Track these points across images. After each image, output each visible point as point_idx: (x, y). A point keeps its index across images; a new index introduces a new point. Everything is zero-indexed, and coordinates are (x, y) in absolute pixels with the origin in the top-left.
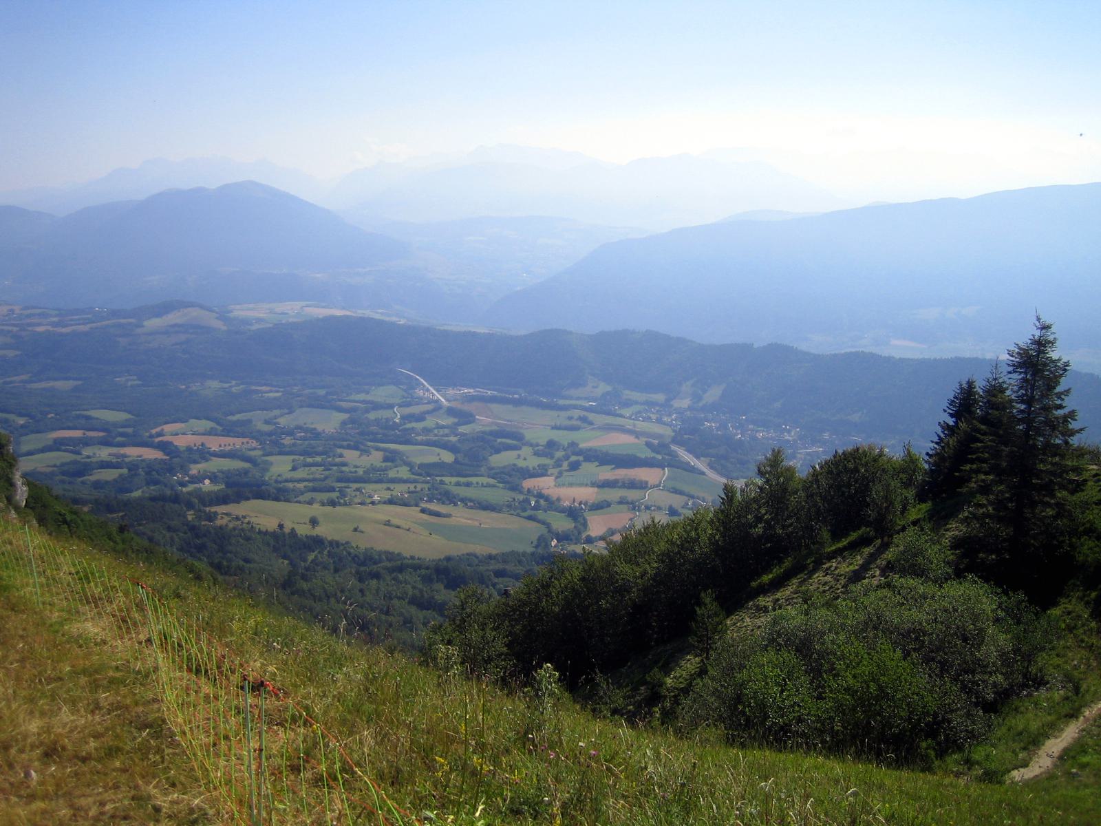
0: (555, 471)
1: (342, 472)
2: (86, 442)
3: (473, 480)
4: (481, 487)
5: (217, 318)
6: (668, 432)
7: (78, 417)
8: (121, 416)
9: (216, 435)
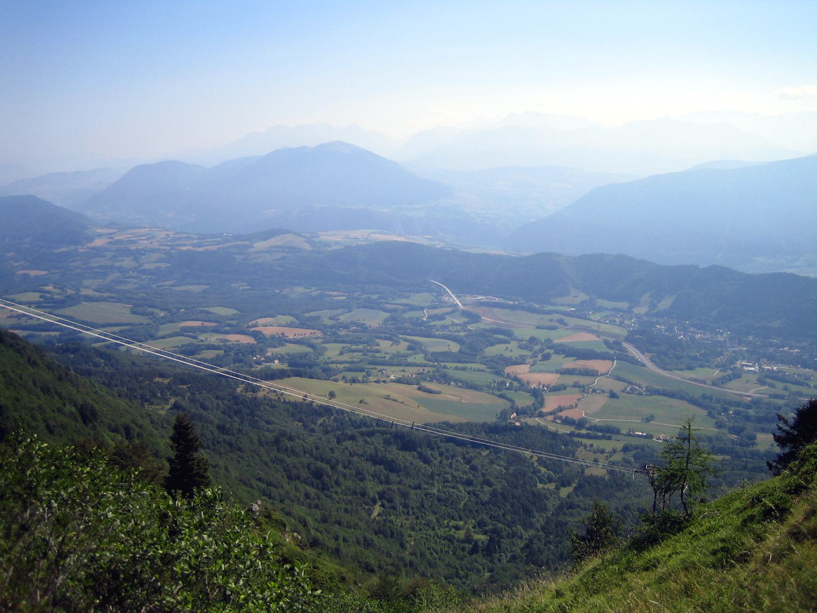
0: (531, 361)
1: (374, 357)
2: (203, 330)
3: (468, 365)
4: (476, 372)
5: (305, 242)
6: (624, 332)
7: (201, 312)
8: (231, 312)
9: (293, 327)
